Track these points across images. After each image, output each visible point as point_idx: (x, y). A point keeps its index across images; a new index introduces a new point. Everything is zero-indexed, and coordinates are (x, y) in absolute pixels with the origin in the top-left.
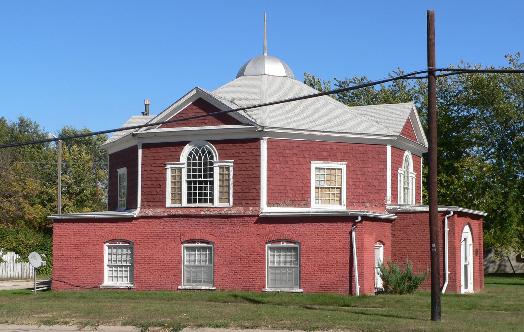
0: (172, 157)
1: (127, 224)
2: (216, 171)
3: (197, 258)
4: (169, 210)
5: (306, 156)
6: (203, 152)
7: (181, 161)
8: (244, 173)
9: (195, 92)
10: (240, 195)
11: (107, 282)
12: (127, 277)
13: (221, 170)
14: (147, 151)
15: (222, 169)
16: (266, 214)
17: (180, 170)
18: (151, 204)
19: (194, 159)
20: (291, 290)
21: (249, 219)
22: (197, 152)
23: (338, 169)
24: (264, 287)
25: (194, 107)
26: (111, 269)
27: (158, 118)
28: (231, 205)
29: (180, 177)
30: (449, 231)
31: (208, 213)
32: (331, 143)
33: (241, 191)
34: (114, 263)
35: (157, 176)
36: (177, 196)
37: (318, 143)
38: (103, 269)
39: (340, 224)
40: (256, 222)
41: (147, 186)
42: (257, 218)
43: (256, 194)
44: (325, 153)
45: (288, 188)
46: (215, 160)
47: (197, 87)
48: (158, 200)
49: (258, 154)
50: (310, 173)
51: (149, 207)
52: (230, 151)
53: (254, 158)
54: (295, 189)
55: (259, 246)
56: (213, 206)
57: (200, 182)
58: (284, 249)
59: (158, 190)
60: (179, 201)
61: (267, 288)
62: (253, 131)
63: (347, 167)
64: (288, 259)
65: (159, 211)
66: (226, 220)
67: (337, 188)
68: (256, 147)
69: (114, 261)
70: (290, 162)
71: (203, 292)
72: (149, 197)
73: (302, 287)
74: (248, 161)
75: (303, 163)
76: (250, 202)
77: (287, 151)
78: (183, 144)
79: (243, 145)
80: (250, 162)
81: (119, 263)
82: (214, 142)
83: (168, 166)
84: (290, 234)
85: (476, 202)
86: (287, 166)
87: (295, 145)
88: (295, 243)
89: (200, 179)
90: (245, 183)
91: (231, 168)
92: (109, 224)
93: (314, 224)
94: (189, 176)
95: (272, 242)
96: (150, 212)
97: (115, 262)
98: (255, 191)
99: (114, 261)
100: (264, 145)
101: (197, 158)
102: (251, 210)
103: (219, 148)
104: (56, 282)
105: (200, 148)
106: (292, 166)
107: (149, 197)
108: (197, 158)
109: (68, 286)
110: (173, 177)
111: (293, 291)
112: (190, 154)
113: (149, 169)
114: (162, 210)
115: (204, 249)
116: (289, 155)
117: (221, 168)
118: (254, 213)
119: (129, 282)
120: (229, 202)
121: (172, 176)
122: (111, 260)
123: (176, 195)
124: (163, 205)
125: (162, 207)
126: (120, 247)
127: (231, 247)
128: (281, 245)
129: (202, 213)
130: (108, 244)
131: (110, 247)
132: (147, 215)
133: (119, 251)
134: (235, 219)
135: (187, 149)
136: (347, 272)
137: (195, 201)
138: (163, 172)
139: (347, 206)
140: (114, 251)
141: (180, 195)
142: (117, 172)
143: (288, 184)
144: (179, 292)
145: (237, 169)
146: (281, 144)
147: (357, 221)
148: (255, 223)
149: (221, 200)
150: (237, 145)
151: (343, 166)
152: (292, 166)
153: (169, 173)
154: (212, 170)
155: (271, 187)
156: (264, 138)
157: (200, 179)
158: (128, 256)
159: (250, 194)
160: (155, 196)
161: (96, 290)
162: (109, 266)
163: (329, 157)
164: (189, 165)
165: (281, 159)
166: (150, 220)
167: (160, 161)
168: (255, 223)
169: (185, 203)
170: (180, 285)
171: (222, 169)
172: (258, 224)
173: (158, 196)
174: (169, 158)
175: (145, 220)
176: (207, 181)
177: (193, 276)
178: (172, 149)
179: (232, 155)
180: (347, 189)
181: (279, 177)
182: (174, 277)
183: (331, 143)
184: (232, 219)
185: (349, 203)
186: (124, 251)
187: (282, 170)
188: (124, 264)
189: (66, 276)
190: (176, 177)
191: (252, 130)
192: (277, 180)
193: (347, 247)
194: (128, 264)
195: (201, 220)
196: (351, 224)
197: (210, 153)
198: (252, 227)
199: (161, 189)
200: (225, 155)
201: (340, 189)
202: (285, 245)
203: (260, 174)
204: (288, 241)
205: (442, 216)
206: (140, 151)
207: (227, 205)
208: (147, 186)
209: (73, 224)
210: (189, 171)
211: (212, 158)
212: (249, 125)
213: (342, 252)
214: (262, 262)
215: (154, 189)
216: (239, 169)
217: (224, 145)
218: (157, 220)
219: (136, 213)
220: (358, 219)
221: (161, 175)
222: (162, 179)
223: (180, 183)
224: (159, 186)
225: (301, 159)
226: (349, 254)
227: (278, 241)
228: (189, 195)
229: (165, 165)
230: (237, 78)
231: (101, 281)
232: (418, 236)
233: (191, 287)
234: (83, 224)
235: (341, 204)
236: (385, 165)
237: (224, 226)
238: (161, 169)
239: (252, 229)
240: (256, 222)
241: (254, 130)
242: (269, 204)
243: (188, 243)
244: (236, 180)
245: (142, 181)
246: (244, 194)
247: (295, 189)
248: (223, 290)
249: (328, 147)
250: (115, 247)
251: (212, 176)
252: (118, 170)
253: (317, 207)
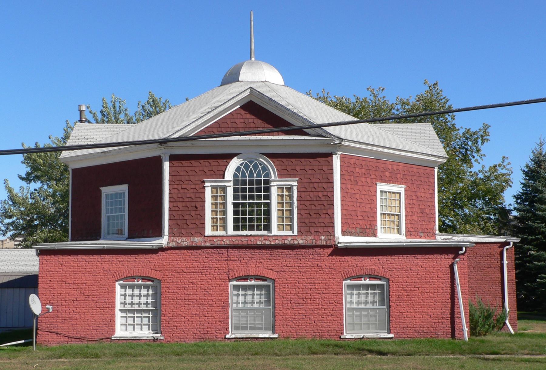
0: (213, 173)
1: (149, 257)
2: (274, 192)
3: (249, 299)
4: (211, 238)
5: (373, 176)
6: (256, 167)
7: (226, 178)
8: (311, 194)
9: (248, 93)
10: (307, 221)
11: (120, 332)
12: (149, 325)
13: (214, 190)
14: (176, 163)
15: (282, 191)
16: (348, 245)
17: (224, 189)
18: (184, 231)
19: (244, 175)
20: (379, 336)
21: (322, 250)
22: (247, 167)
23: (398, 193)
24: (342, 333)
25: (243, 112)
26: (124, 315)
27: (196, 122)
28: (296, 233)
29: (225, 197)
30: (508, 264)
31: (268, 243)
32: (392, 163)
33: (309, 216)
34: (128, 307)
35: (192, 196)
36: (220, 221)
37: (385, 163)
38: (114, 315)
39: (438, 256)
40: (331, 255)
41: (177, 209)
42: (332, 249)
43: (328, 220)
44: (388, 174)
45: (359, 214)
46: (273, 178)
47: (251, 88)
48: (194, 226)
49: (330, 171)
50: (376, 196)
51: (181, 234)
52: (293, 167)
53: (324, 176)
54: (364, 214)
55: (335, 284)
56: (270, 234)
57: (251, 205)
58: (367, 287)
59: (193, 213)
60: (221, 228)
61: (345, 334)
62: (328, 144)
63: (405, 191)
64: (370, 298)
65: (197, 240)
66: (291, 252)
67: (397, 215)
68: (327, 163)
69: (129, 304)
70: (360, 183)
71: (260, 341)
72: (179, 222)
73: (392, 331)
74: (318, 181)
75: (370, 184)
76: (320, 230)
77: (357, 170)
78: (230, 157)
79: (310, 160)
80: (319, 181)
81: (136, 307)
82: (271, 156)
83: (206, 184)
84: (376, 268)
85: (21, 221)
86: (357, 187)
87: (363, 163)
88: (380, 280)
89: (251, 201)
90: (313, 207)
91: (295, 188)
92: (124, 257)
93: (405, 256)
94: (235, 197)
95: (352, 278)
96: (184, 242)
97: (130, 306)
98: (327, 216)
99: (129, 304)
100: (336, 161)
101: (247, 175)
102: (323, 239)
103: (278, 163)
104: (43, 333)
105: (251, 163)
106: (361, 188)
107: (179, 222)
108: (247, 175)
109: (63, 339)
110: (214, 197)
111: (382, 337)
112: (238, 169)
113: (179, 187)
114: (201, 239)
115: (259, 287)
116: (358, 175)
117: (280, 188)
118: (329, 243)
119: (151, 332)
120: (292, 229)
121: (213, 196)
122: (124, 304)
123: (218, 222)
124: (201, 232)
125: (199, 234)
126: (139, 287)
127: (297, 284)
128: (363, 282)
129: (259, 243)
130: (121, 282)
131: (122, 287)
132: (179, 245)
133: (136, 292)
134: (304, 250)
135: (235, 163)
136: (448, 312)
137: (244, 228)
138: (201, 190)
139: (406, 236)
140: (129, 292)
141: (225, 220)
142: (101, 191)
143: (358, 209)
144: (228, 342)
145: (302, 189)
146: (352, 161)
147: (460, 252)
148: (329, 255)
149: (281, 227)
150: (303, 160)
151: (401, 189)
152: (361, 188)
153: (208, 192)
154: (268, 189)
155: (345, 212)
156: (338, 153)
157: (251, 201)
158: (150, 298)
159: (321, 220)
160: (189, 217)
161: (106, 343)
162: (121, 311)
163: (391, 179)
164: (236, 182)
165: (352, 178)
166: (185, 251)
167: (197, 178)
168: (329, 255)
169: (231, 231)
170: (228, 334)
171: (282, 191)
172: (334, 257)
173: (193, 222)
174: (208, 173)
175: (177, 251)
176: (239, 203)
177: (243, 322)
178: (213, 162)
179: (295, 172)
180: (406, 216)
181: (351, 200)
182: (219, 323)
183: (392, 163)
184: (299, 250)
185: (409, 234)
186: (144, 292)
187: (353, 192)
188: (143, 307)
189: (59, 325)
190: (217, 198)
191: (326, 142)
192: (349, 204)
193: (447, 283)
194: (150, 307)
195: (257, 251)
196: (451, 256)
197: (265, 168)
198: (325, 259)
199: (198, 212)
200: (286, 172)
201: (399, 216)
202: (368, 282)
203: (333, 196)
204: (371, 277)
205: (500, 247)
206: (166, 165)
207: (289, 233)
208: (177, 209)
209: (69, 257)
210: (235, 190)
211: (268, 175)
212: (322, 136)
213: (440, 288)
214: (339, 303)
215: (188, 213)
216: (305, 190)
217: (284, 160)
218: (194, 252)
219: (164, 241)
220: (462, 250)
221: (197, 195)
222: (199, 200)
223: (225, 205)
224: (195, 208)
225: (369, 180)
226: (449, 291)
227: (359, 277)
228: (236, 220)
229: (204, 182)
230: (221, 85)
231: (113, 330)
232: (473, 270)
233: (244, 336)
234: (84, 257)
235: (399, 232)
236: (434, 190)
237: (288, 259)
238: (197, 187)
239: (326, 262)
240: (331, 255)
241: (329, 142)
242: (344, 233)
243: (236, 281)
244: (302, 202)
245: (170, 202)
246: (312, 220)
247: (364, 214)
248: (288, 338)
249: (390, 167)
250: (132, 287)
251: (268, 197)
252: (101, 188)
253: (386, 237)
